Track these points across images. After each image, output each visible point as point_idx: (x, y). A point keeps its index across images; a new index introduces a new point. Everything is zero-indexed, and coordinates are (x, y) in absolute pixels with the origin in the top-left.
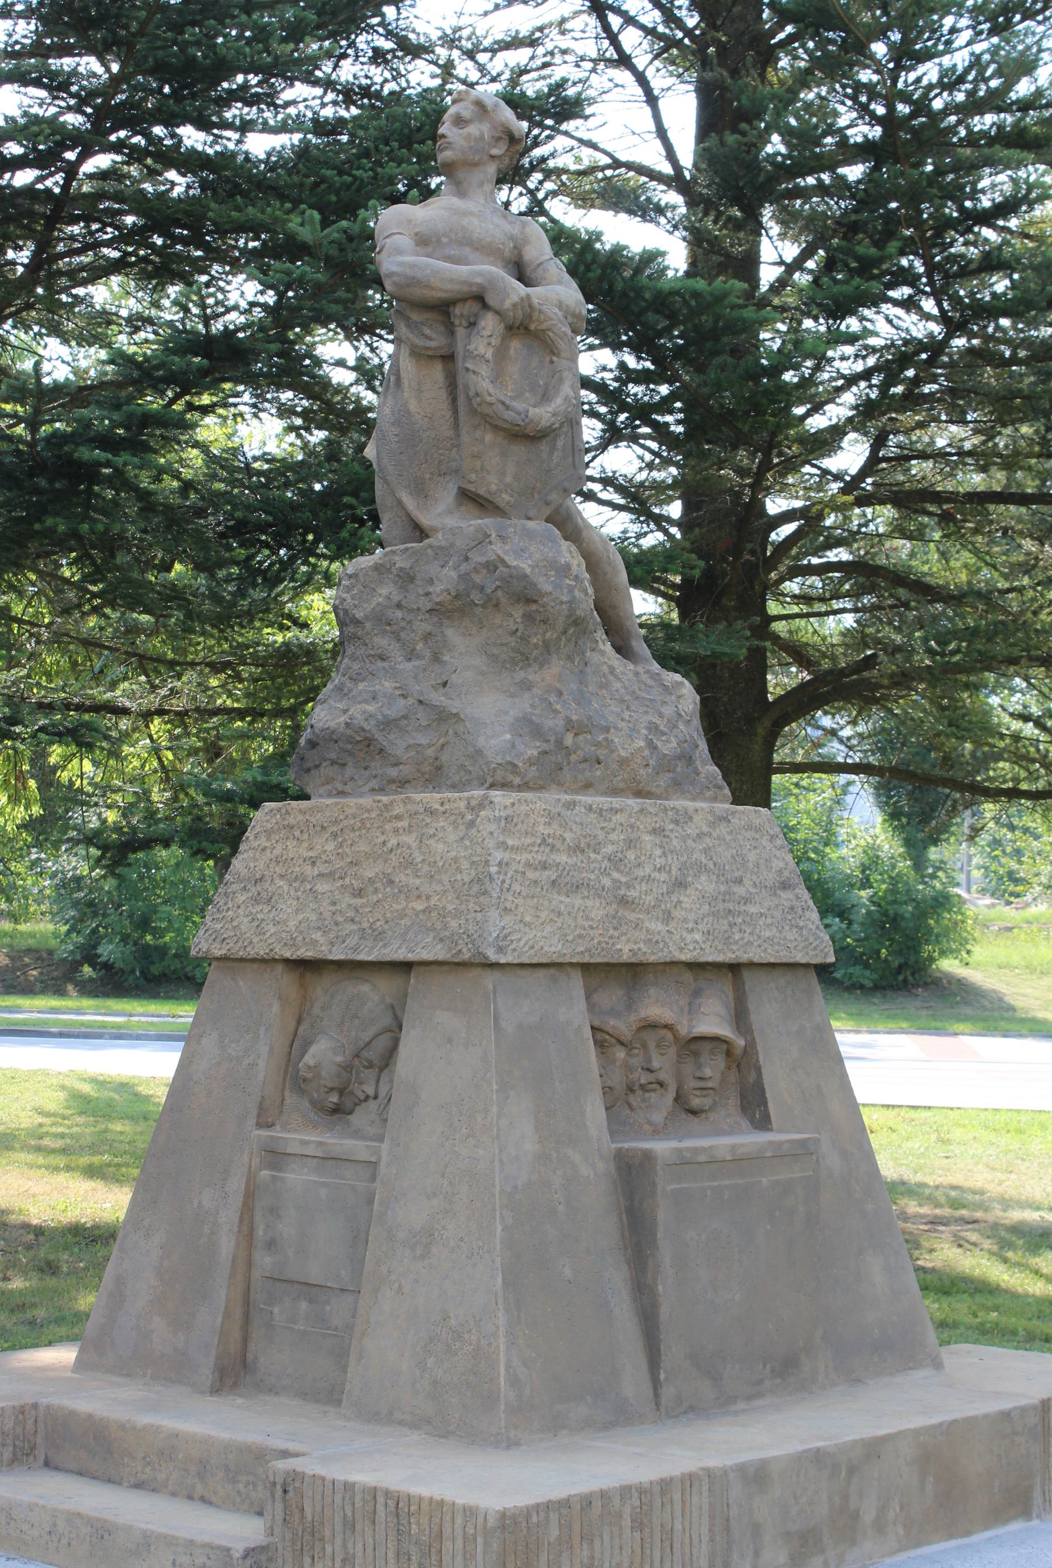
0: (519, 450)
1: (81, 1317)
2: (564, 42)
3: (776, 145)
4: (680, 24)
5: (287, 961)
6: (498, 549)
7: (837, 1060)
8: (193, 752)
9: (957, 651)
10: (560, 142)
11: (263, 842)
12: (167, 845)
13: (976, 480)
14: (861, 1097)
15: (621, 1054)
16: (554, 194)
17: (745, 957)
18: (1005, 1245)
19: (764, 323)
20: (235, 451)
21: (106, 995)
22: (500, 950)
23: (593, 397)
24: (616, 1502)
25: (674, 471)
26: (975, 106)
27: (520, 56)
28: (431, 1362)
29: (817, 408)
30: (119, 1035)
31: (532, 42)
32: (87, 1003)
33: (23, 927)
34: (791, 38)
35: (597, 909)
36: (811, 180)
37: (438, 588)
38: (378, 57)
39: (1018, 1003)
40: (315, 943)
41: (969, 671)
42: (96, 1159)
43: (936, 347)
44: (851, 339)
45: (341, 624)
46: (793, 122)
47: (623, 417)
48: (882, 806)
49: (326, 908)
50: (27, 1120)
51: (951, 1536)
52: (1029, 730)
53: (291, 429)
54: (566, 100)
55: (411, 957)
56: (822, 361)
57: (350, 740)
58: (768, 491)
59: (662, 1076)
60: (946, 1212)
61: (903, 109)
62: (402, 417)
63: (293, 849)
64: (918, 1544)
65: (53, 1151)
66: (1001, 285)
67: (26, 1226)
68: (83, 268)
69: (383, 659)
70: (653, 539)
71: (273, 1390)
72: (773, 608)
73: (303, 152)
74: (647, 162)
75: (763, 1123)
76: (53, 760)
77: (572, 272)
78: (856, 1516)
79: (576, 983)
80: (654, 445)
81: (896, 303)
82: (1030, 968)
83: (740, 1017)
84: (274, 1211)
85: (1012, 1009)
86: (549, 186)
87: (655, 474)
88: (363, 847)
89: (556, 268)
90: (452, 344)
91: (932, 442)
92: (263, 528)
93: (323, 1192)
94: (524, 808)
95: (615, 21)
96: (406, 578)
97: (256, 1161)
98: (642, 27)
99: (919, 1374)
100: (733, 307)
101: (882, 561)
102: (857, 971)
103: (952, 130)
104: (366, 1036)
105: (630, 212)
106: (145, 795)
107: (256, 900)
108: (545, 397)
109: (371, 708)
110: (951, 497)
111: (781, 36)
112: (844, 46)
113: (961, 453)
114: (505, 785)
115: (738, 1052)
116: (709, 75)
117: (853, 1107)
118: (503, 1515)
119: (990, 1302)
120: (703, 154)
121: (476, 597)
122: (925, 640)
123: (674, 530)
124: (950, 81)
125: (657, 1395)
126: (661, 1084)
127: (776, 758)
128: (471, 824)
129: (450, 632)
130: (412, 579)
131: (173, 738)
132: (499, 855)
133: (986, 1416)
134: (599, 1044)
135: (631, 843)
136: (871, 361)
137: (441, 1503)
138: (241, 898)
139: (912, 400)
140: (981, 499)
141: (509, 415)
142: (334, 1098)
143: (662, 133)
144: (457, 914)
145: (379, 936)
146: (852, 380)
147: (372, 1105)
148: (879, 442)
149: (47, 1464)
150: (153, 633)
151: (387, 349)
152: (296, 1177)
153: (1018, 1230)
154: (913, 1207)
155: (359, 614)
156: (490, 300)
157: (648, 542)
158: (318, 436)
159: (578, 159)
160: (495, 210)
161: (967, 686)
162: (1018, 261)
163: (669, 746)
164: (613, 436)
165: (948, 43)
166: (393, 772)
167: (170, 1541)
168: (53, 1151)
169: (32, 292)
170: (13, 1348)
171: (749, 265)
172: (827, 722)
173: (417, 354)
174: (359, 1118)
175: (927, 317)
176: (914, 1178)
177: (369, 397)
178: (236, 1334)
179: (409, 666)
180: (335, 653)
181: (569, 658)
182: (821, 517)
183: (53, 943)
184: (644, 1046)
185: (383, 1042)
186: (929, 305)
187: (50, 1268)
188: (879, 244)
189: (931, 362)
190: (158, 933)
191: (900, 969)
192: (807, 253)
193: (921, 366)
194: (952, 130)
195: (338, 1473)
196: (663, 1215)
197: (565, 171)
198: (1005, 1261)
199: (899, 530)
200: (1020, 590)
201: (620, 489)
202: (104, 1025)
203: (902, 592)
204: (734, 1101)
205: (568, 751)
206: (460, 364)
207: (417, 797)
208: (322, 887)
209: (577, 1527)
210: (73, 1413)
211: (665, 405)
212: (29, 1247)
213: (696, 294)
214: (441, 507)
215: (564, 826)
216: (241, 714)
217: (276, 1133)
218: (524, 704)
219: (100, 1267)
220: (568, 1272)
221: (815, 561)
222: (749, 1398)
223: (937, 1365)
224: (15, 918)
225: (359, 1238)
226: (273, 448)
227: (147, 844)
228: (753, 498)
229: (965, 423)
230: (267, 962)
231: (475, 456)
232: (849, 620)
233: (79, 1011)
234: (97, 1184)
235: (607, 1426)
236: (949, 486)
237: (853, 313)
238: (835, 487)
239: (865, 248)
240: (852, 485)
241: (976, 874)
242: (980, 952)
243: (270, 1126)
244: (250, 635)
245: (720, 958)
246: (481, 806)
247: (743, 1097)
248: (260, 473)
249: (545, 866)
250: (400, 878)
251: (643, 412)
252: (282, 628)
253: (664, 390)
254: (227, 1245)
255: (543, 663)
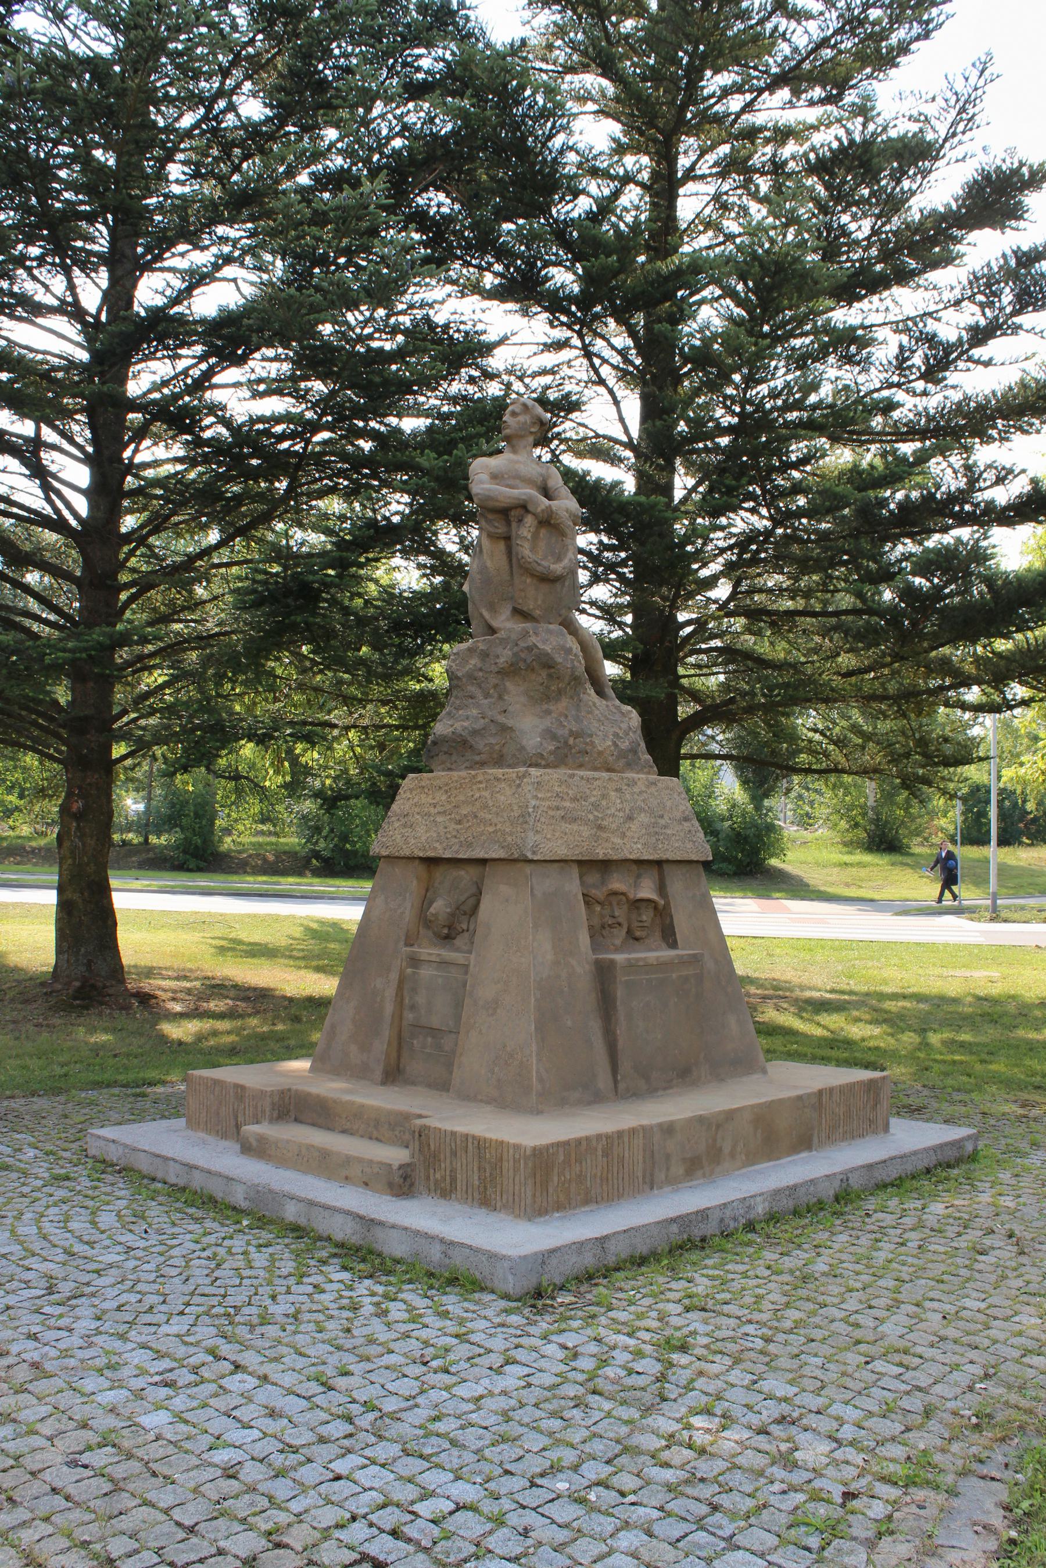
0: (545, 587)
1: (313, 1045)
2: (570, 372)
3: (682, 426)
4: (631, 363)
5: (420, 858)
6: (533, 639)
7: (714, 912)
8: (372, 748)
9: (779, 695)
10: (568, 425)
11: (408, 795)
12: (357, 798)
13: (789, 604)
14: (726, 931)
15: (598, 908)
16: (564, 451)
17: (664, 857)
18: (801, 1009)
19: (676, 519)
20: (393, 587)
21: (326, 876)
22: (534, 853)
23: (585, 559)
24: (594, 1142)
25: (628, 598)
26: (787, 408)
27: (547, 379)
28: (496, 1069)
29: (705, 565)
30: (332, 898)
31: (552, 372)
32: (316, 880)
33: (282, 840)
34: (690, 371)
35: (586, 831)
36: (701, 445)
37: (502, 660)
38: (472, 380)
39: (811, 882)
40: (435, 849)
41: (786, 705)
42: (321, 963)
43: (768, 533)
44: (722, 528)
45: (450, 679)
46: (691, 414)
47: (601, 569)
48: (739, 777)
49: (442, 830)
50: (284, 942)
51: (770, 1160)
52: (817, 737)
53: (424, 575)
54: (571, 403)
55: (486, 856)
56: (707, 540)
57: (454, 741)
58: (678, 609)
59: (620, 920)
60: (771, 992)
61: (749, 408)
62: (483, 570)
63: (425, 799)
64: (753, 1164)
65: (298, 958)
66: (802, 501)
67: (284, 997)
68: (315, 491)
69: (472, 697)
70: (617, 634)
71: (413, 1083)
72: (681, 671)
73: (430, 429)
74: (614, 435)
75: (673, 945)
76: (297, 751)
77: (574, 492)
78: (720, 1150)
79: (575, 871)
80: (617, 584)
81: (746, 510)
82: (817, 864)
83: (662, 889)
84: (414, 990)
85: (808, 885)
86: (562, 447)
87: (618, 600)
88: (462, 798)
89: (565, 491)
90: (510, 530)
91: (765, 584)
92: (408, 626)
93: (440, 981)
94: (547, 778)
95: (597, 362)
96: (485, 655)
97: (404, 964)
98: (612, 365)
99: (755, 1076)
100: (660, 511)
101: (738, 646)
102: (724, 865)
103: (776, 420)
104: (463, 898)
105: (605, 461)
106: (346, 771)
107: (405, 826)
108: (559, 559)
109: (466, 724)
110: (776, 613)
111: (686, 370)
112: (717, 376)
113: (781, 590)
114: (537, 765)
115: (661, 907)
116: (646, 390)
117: (722, 938)
118: (534, 1149)
119: (793, 1039)
120: (643, 430)
121: (522, 665)
122: (762, 689)
123: (628, 630)
124: (774, 395)
125: (616, 1087)
126: (619, 924)
127: (683, 751)
128: (519, 786)
129: (508, 684)
130: (488, 655)
131: (361, 740)
132: (533, 802)
133: (789, 1098)
134: (587, 903)
135: (604, 796)
136: (732, 541)
137: (502, 1142)
138: (396, 825)
139: (755, 561)
140: (791, 614)
141: (539, 569)
142: (446, 931)
143: (622, 420)
144: (511, 834)
145: (470, 845)
146: (722, 551)
147: (466, 934)
148: (737, 584)
149: (296, 1120)
150: (350, 684)
151: (475, 533)
152: (426, 973)
153: (809, 1002)
154: (753, 990)
155: (460, 674)
156: (530, 508)
157: (614, 635)
158: (438, 580)
159: (577, 433)
160: (533, 460)
161: (783, 714)
162: (811, 489)
163: (625, 745)
164: (595, 579)
165: (773, 374)
166: (477, 758)
167: (360, 1160)
168: (298, 958)
169: (288, 505)
170: (278, 1060)
171: (668, 489)
172: (709, 732)
173: (491, 536)
174: (459, 942)
175: (762, 517)
176: (755, 975)
177: (466, 559)
178: (394, 1054)
179: (486, 701)
180: (447, 695)
181: (572, 698)
182: (706, 623)
183: (298, 848)
184: (611, 904)
185: (472, 901)
186: (764, 511)
187: (297, 1019)
188: (738, 479)
189: (766, 541)
190: (354, 843)
191: (748, 864)
192: (699, 484)
193: (760, 544)
194: (776, 420)
195: (448, 1126)
196: (620, 993)
197: (570, 439)
198: (802, 1018)
199: (748, 630)
200: (812, 662)
201: (599, 608)
202: (324, 892)
203: (750, 663)
204: (658, 934)
205: (571, 748)
206: (513, 542)
207: (490, 771)
208: (439, 819)
209: (573, 1156)
210: (309, 1094)
211: (623, 563)
212: (286, 1008)
213: (640, 504)
214: (503, 617)
215: (568, 786)
216: (397, 728)
217: (415, 949)
218: (547, 723)
219: (322, 1018)
220: (569, 1023)
221: (704, 646)
222: (665, 1089)
223: (764, 1071)
224: (276, 834)
225: (458, 1005)
226: (416, 587)
227: (347, 798)
228: (671, 612)
229: (783, 573)
230: (411, 859)
231: (522, 590)
232: (722, 678)
233: (311, 885)
234: (322, 976)
235: (589, 1103)
236: (775, 607)
237: (724, 515)
238: (714, 607)
239: (730, 481)
240: (723, 606)
241: (789, 813)
242: (790, 855)
243: (412, 945)
244: (402, 685)
245: (651, 858)
246: (524, 776)
247: (663, 931)
248: (407, 599)
249: (558, 808)
250: (481, 814)
251: (611, 567)
252: (419, 681)
253: (623, 555)
254: (389, 1008)
255: (557, 700)
